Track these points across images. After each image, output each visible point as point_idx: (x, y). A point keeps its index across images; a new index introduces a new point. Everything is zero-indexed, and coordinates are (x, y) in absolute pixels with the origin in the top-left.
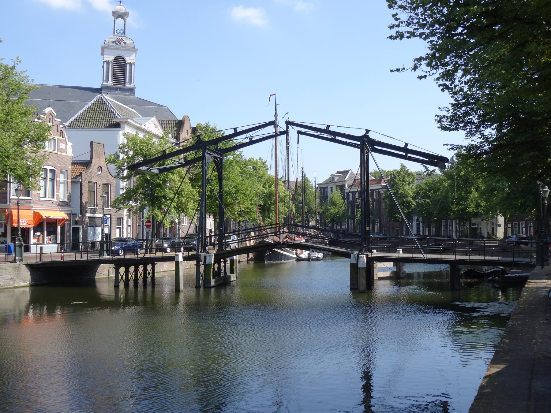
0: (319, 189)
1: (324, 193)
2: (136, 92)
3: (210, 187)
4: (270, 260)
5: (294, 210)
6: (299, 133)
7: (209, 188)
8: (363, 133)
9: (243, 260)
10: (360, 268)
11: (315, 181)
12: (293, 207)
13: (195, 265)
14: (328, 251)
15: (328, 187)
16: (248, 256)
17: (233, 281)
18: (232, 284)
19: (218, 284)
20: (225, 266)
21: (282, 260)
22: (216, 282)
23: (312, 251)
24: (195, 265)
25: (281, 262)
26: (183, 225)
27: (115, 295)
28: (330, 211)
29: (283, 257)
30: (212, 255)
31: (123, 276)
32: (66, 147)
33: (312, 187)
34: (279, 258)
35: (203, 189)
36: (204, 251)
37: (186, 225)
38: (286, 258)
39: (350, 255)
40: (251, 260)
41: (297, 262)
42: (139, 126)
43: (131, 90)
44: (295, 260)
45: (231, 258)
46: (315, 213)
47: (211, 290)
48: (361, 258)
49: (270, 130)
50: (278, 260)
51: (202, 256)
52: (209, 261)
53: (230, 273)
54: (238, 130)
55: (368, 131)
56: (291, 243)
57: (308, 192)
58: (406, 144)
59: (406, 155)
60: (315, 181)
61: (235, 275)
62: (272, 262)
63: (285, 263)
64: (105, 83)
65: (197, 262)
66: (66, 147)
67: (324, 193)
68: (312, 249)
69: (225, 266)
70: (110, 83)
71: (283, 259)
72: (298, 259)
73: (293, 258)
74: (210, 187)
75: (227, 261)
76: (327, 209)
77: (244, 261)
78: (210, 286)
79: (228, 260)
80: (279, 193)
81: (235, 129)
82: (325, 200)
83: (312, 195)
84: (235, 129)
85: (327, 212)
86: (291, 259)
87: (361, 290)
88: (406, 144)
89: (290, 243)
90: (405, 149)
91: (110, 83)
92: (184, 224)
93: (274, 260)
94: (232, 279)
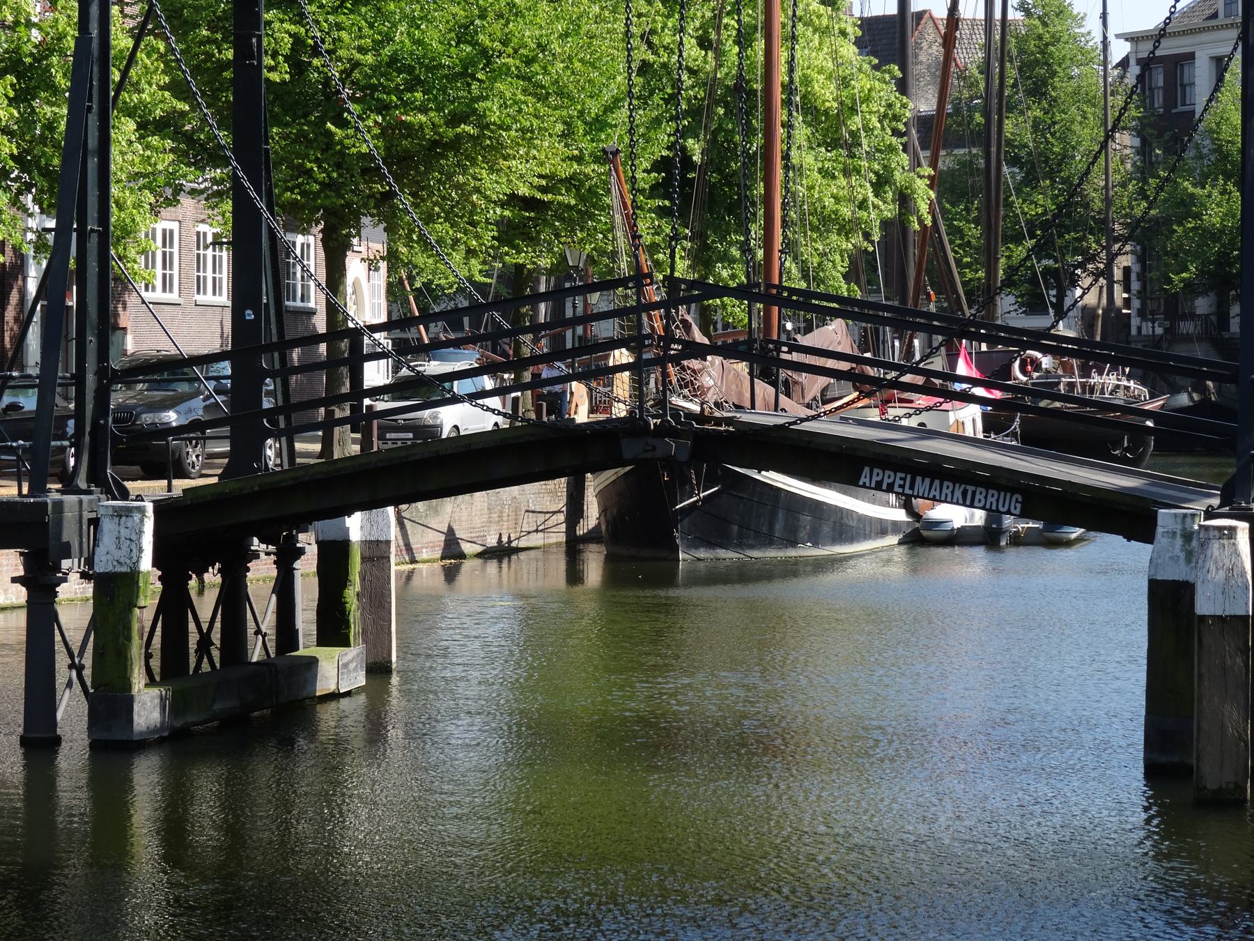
0: (1134, 70)
1: (1170, 100)
3: (293, 28)
4: (711, 545)
5: (924, 207)
7: (287, 39)
9: (536, 540)
10: (1203, 618)
11: (1104, 16)
12: (921, 185)
13: (14, 580)
14: (999, 488)
15: (1191, 56)
16: (575, 510)
17: (335, 696)
18: (327, 716)
19: (178, 724)
20: (284, 588)
21: (793, 543)
22: (175, 706)
23: (878, 487)
24: (14, 580)
25: (792, 553)
26: (201, 298)
28: (1198, 216)
29: (806, 519)
30: (142, 511)
33: (1084, 58)
34: (779, 527)
36: (90, 480)
37: (173, 297)
38: (826, 529)
39: (1152, 521)
40: (593, 537)
41: (911, 554)
44: (893, 540)
45: (326, 527)
46: (1103, 226)
47: (128, 766)
48: (1215, 547)
50: (768, 540)
51: (69, 515)
52: (121, 554)
53: (323, 640)
56: (729, 421)
57: (1060, 88)
60: (1104, 16)
61: (354, 654)
62: (728, 555)
63: (821, 566)
65: (28, 561)
67: (1170, 100)
68: (878, 474)
69: (284, 588)
71: (803, 534)
72: (916, 532)
73: (883, 528)
74: (293, 28)
75: (301, 552)
76: (1182, 203)
77: (545, 549)
78: (119, 735)
79: (308, 541)
80: (807, 81)
82: (1176, 147)
83: (1089, 110)
85: (1180, 224)
86: (867, 537)
87: (1211, 785)
89: (719, 421)
92: (158, 295)
93: (740, 545)
94: (327, 680)
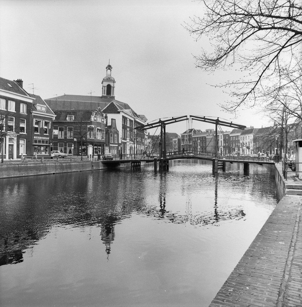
2: (115, 98)
6: (192, 119)
8: (216, 119)
27: (154, 169)
31: (185, 154)
32: (104, 120)
35: (40, 146)
42: (126, 113)
43: (113, 97)
49: (186, 118)
54: (174, 118)
55: (218, 118)
58: (232, 122)
59: (152, 126)
63: (114, 225)
64: (103, 95)
66: (104, 120)
70: (105, 95)
81: (173, 117)
84: (173, 117)
88: (232, 122)
90: (204, 118)
91: (105, 95)
